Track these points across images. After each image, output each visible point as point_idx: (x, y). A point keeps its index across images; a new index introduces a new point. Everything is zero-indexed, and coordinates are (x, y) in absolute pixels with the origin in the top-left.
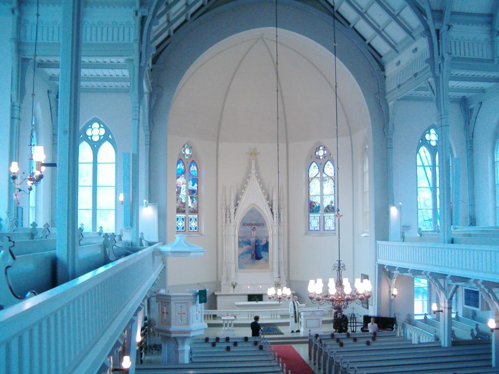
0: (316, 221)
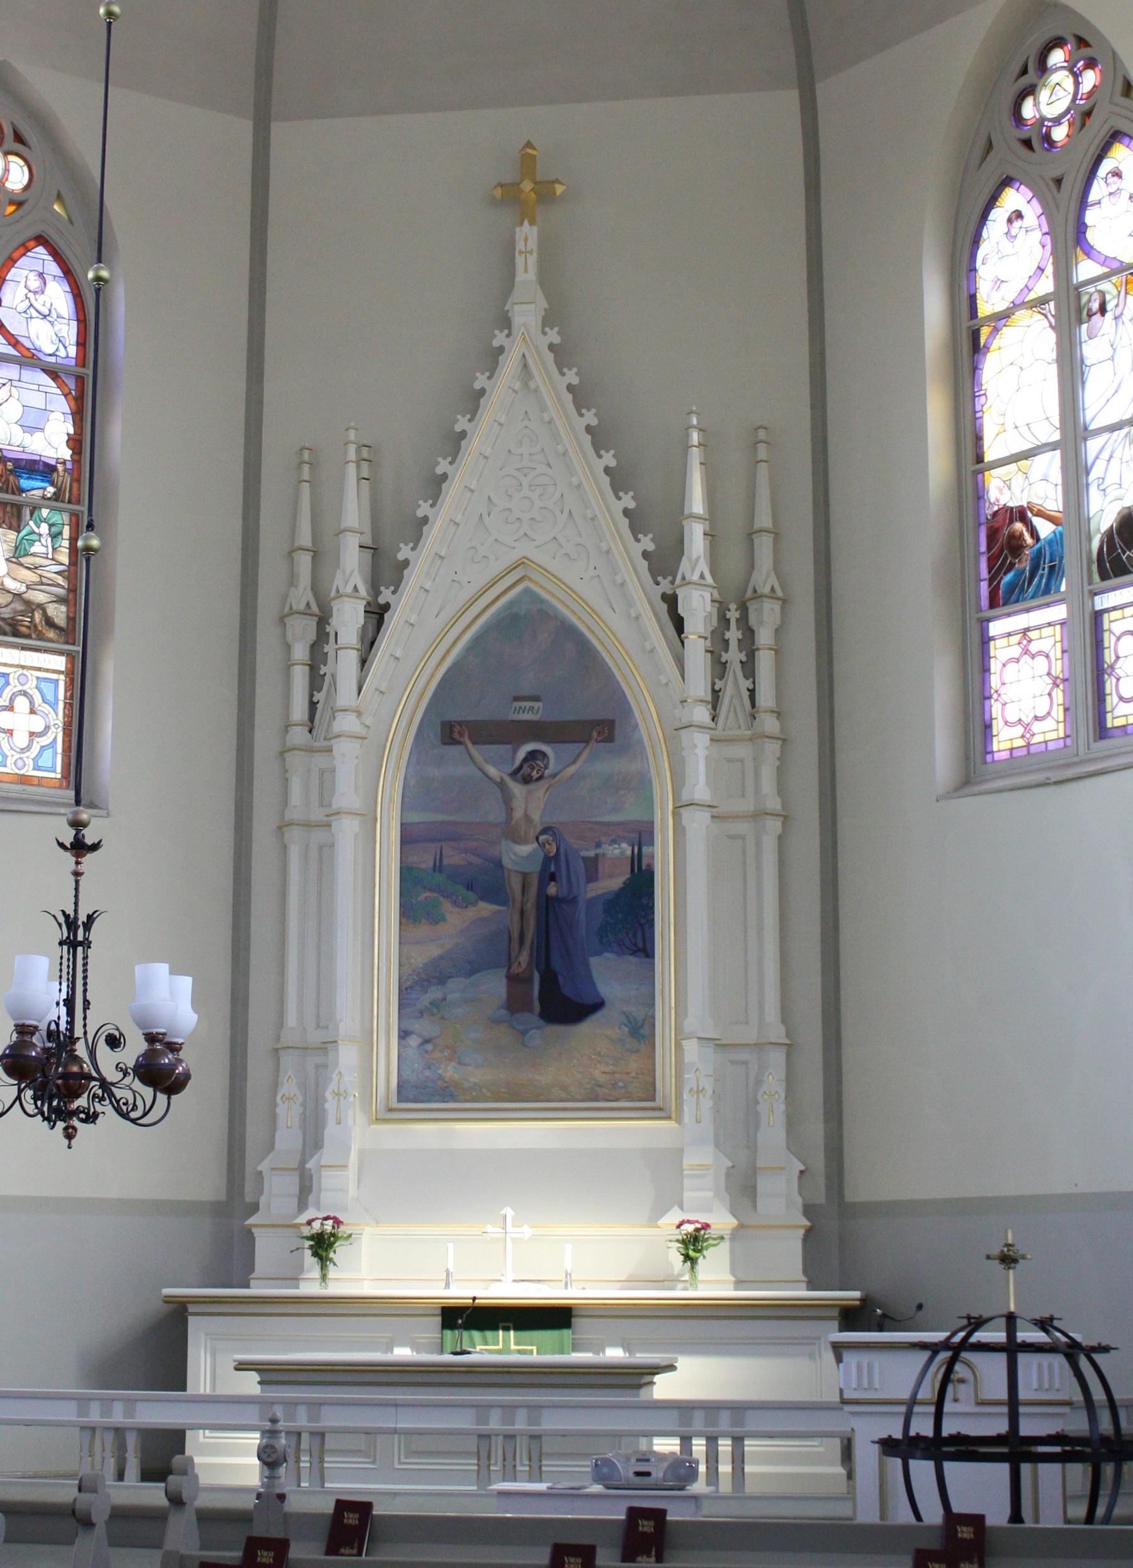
0: (1041, 663)
